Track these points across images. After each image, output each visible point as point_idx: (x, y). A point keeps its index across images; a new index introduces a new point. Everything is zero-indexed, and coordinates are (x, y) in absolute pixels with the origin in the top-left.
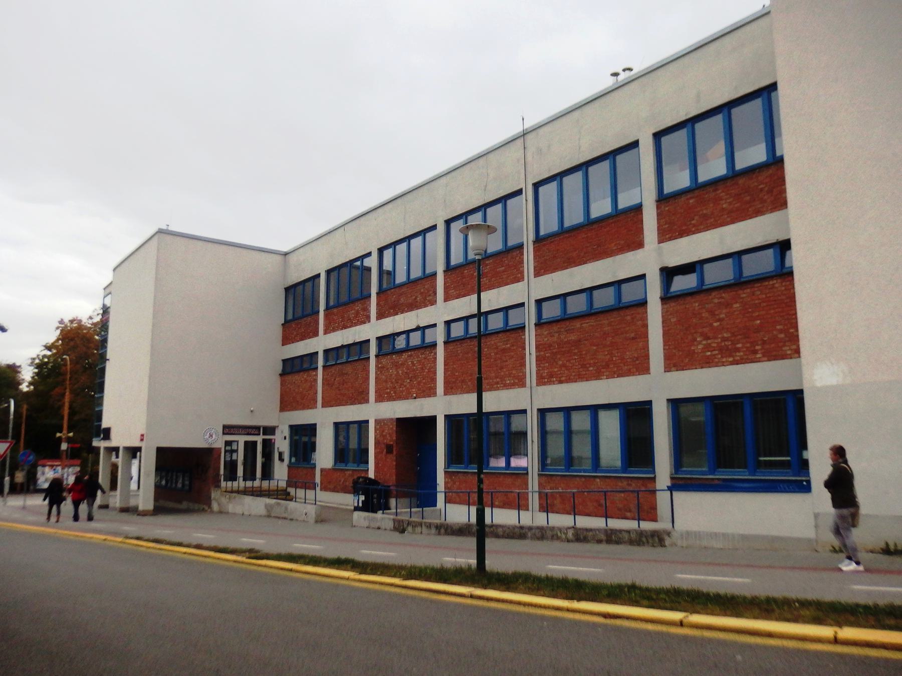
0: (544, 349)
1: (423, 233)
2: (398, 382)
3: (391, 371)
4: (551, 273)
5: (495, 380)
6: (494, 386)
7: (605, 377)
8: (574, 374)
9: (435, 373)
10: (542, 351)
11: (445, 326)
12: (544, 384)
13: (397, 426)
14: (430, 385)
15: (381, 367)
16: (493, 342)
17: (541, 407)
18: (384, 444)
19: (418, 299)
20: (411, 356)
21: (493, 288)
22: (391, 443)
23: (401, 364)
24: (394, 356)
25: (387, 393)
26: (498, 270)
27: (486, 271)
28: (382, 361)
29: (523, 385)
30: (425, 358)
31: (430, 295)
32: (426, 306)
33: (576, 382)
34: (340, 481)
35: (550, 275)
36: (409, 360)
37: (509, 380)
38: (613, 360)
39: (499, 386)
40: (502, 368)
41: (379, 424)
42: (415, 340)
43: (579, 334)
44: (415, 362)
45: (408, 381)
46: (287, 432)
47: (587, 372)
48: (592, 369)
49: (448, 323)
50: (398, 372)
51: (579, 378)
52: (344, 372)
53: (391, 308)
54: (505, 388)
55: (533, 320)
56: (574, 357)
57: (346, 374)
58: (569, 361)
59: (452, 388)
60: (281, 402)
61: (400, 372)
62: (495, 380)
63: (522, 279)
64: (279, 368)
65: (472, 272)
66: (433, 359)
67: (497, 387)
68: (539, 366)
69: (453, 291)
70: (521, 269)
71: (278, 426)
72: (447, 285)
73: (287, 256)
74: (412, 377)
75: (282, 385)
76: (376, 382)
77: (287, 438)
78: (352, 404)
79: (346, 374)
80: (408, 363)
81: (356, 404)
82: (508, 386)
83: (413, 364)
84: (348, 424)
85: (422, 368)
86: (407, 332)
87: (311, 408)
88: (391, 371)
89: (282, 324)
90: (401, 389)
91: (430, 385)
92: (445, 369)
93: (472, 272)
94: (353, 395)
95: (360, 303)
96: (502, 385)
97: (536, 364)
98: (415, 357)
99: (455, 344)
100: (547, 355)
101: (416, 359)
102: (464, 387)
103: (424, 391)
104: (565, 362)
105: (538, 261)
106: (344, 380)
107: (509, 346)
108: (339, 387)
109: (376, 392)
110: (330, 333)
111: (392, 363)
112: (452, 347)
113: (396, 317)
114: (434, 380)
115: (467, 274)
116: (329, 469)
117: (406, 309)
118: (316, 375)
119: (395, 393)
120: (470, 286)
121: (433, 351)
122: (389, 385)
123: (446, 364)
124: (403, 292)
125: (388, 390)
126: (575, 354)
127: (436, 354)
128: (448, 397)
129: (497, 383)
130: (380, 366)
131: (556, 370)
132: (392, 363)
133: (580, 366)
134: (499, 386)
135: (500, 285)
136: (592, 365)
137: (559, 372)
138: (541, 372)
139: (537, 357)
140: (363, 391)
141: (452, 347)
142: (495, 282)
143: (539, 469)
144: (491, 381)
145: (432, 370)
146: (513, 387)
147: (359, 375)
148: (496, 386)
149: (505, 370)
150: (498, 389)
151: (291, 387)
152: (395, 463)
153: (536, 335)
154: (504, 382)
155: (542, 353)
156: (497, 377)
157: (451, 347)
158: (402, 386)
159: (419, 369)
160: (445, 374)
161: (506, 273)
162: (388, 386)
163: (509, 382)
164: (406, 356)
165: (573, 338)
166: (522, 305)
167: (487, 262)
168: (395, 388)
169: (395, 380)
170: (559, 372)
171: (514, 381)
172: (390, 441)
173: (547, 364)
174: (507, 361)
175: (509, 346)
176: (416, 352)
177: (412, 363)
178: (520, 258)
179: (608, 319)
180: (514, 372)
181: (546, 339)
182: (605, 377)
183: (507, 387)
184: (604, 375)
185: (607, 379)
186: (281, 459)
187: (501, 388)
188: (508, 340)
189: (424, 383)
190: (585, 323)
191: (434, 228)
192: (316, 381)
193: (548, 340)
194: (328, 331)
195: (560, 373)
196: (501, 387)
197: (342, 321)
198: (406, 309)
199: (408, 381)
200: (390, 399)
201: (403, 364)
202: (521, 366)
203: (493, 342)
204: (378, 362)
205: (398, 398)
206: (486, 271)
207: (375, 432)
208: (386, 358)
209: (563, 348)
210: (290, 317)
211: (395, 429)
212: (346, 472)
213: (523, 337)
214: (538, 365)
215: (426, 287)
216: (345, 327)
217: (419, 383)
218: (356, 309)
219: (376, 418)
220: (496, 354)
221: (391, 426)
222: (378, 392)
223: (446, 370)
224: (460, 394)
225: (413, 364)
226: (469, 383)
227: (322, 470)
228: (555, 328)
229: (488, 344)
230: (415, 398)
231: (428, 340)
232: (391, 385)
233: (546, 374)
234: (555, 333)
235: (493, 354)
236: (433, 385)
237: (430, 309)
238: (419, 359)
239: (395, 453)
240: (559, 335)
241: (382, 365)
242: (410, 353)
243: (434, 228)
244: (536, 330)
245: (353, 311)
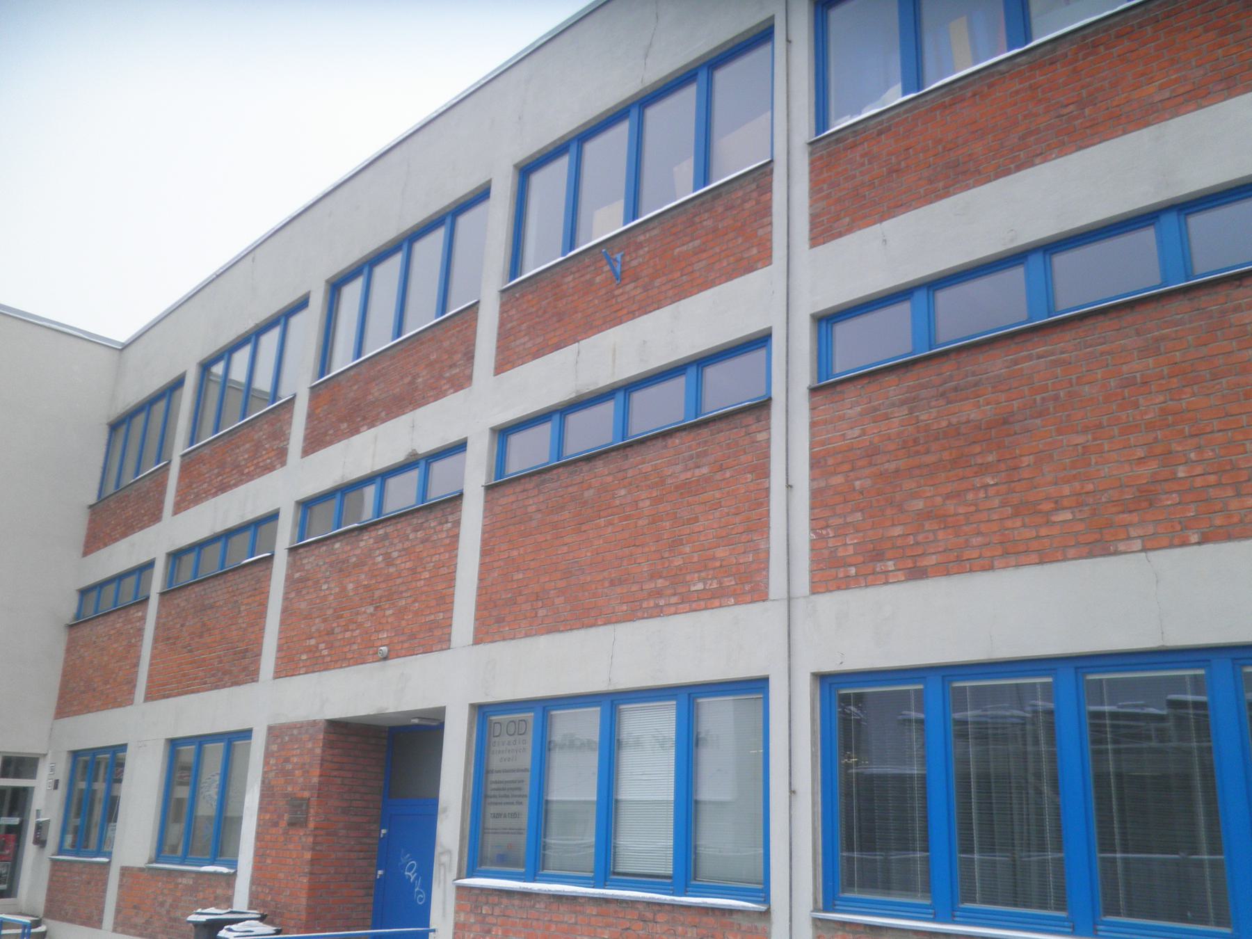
0: (846, 467)
1: (447, 218)
2: (341, 617)
3: (325, 587)
4: (882, 220)
5: (649, 586)
6: (645, 605)
7: (1138, 544)
8: (976, 541)
9: (451, 579)
10: (835, 473)
11: (491, 444)
12: (844, 584)
13: (329, 744)
14: (432, 617)
15: (301, 580)
16: (646, 467)
17: (830, 666)
18: (286, 796)
19: (420, 380)
20: (386, 536)
21: (656, 306)
22: (306, 794)
23: (356, 566)
24: (337, 545)
25: (309, 650)
26: (677, 251)
27: (634, 263)
28: (305, 561)
29: (759, 594)
30: (424, 541)
31: (452, 366)
32: (440, 395)
33: (991, 568)
34: (162, 904)
35: (877, 229)
36: (378, 552)
37: (700, 580)
38: (1175, 478)
39: (662, 602)
40: (676, 543)
41: (279, 741)
42: (402, 494)
43: (1003, 397)
44: (395, 554)
45: (371, 609)
46: (62, 770)
47: (1044, 532)
48: (1067, 516)
49: (503, 433)
50: (344, 589)
51: (1006, 553)
52: (207, 602)
53: (341, 420)
54: (687, 606)
55: (804, 376)
56: (977, 482)
57: (212, 607)
58: (957, 495)
59: (500, 620)
60: (62, 697)
61: (350, 586)
62: (649, 586)
63: (765, 258)
64: (68, 608)
65: (588, 277)
66: (447, 541)
67: (657, 606)
68: (823, 523)
69: (526, 338)
70: (761, 232)
71: (45, 755)
72: (509, 326)
73: (125, 352)
74: (381, 597)
75: (69, 650)
76: (282, 622)
77: (62, 785)
78: (216, 686)
79: (212, 607)
80: (374, 558)
81: (224, 686)
82: (699, 599)
83: (389, 561)
84: (201, 741)
85: (413, 571)
86: (382, 477)
87: (120, 706)
88: (325, 587)
89: (91, 507)
90: (348, 634)
91: (432, 617)
92: (482, 564)
93: (588, 277)
94: (220, 662)
95: (267, 423)
96: (674, 600)
97: (813, 519)
98: (396, 541)
99: (518, 488)
100: (857, 483)
101: (399, 546)
102: (541, 613)
103: (413, 637)
104: (939, 500)
105: (828, 196)
106: (204, 625)
107: (705, 470)
108: (189, 645)
109: (280, 649)
110: (186, 508)
111: (331, 565)
112: (512, 498)
113: (356, 439)
114: (445, 602)
115: (572, 284)
116: (141, 870)
117: (383, 414)
118: (143, 619)
119: (330, 646)
120: (579, 315)
121: (450, 518)
122: (318, 624)
123: (487, 550)
124: (379, 371)
125: (313, 642)
126: (984, 469)
127: (457, 523)
128: (486, 649)
129: (659, 593)
130: (297, 575)
131: (898, 531)
132: (331, 565)
133: (1009, 510)
134: (662, 602)
135: (681, 294)
136: (1066, 503)
137: (911, 540)
138: (831, 543)
139: (816, 494)
140: (247, 650)
141: (512, 498)
142: (664, 288)
143: (815, 901)
144: (635, 588)
145: (444, 571)
146: (716, 602)
147: (243, 608)
148: (652, 603)
149: (687, 549)
150: (658, 612)
151: (86, 654)
152: (308, 855)
153: (813, 424)
154: (680, 590)
155: (838, 480)
156: (654, 576)
157: (507, 498)
158: (352, 626)
159: (405, 573)
160: (481, 579)
161: (705, 255)
162: (313, 629)
163: (700, 586)
164: (372, 541)
165: (974, 415)
166: (762, 340)
167: (641, 238)
168: (330, 632)
169: (335, 611)
170: (911, 540)
171: (720, 583)
172: (303, 790)
173: (859, 516)
174: (696, 520)
175: (705, 470)
176: (399, 526)
177: (387, 556)
178: (758, 202)
179: (1138, 333)
180: (721, 552)
181: (857, 431)
182: (1138, 544)
183: (694, 605)
184: (1129, 538)
185: (1144, 550)
186: (40, 842)
187: (673, 609)
188: (705, 454)
189: (416, 613)
190: (1030, 358)
191: (482, 195)
192: (140, 632)
193: (864, 433)
194: (182, 505)
195: (917, 543)
196: (669, 605)
197: (219, 474)
198: (383, 414)
199: (371, 609)
200: (318, 664)
201: (360, 564)
202: (750, 530)
203: (646, 467)
204: (293, 566)
205: (336, 661)
206: (634, 263)
207: (266, 763)
208: (316, 552)
209: (927, 452)
210: (110, 489)
211: (318, 751)
212: (180, 880)
213: (761, 437)
214: (817, 522)
215: (446, 344)
216: (223, 488)
217: (400, 613)
218: (256, 437)
219: (272, 723)
220: (657, 501)
221: (310, 745)
222: (285, 647)
223: (485, 569)
224: (527, 635)
225: (389, 561)
226: (559, 601)
227: (125, 871)
228: (893, 389)
229: (630, 473)
230: (385, 658)
231: (437, 492)
232: (322, 626)
233: (851, 550)
234: (893, 405)
235: (648, 503)
236: (441, 616)
237: (453, 401)
238: (407, 544)
239: (311, 825)
240: (911, 411)
241: (303, 573)
242: (381, 532)
243: (482, 195)
244: (813, 409)
245: (247, 446)
